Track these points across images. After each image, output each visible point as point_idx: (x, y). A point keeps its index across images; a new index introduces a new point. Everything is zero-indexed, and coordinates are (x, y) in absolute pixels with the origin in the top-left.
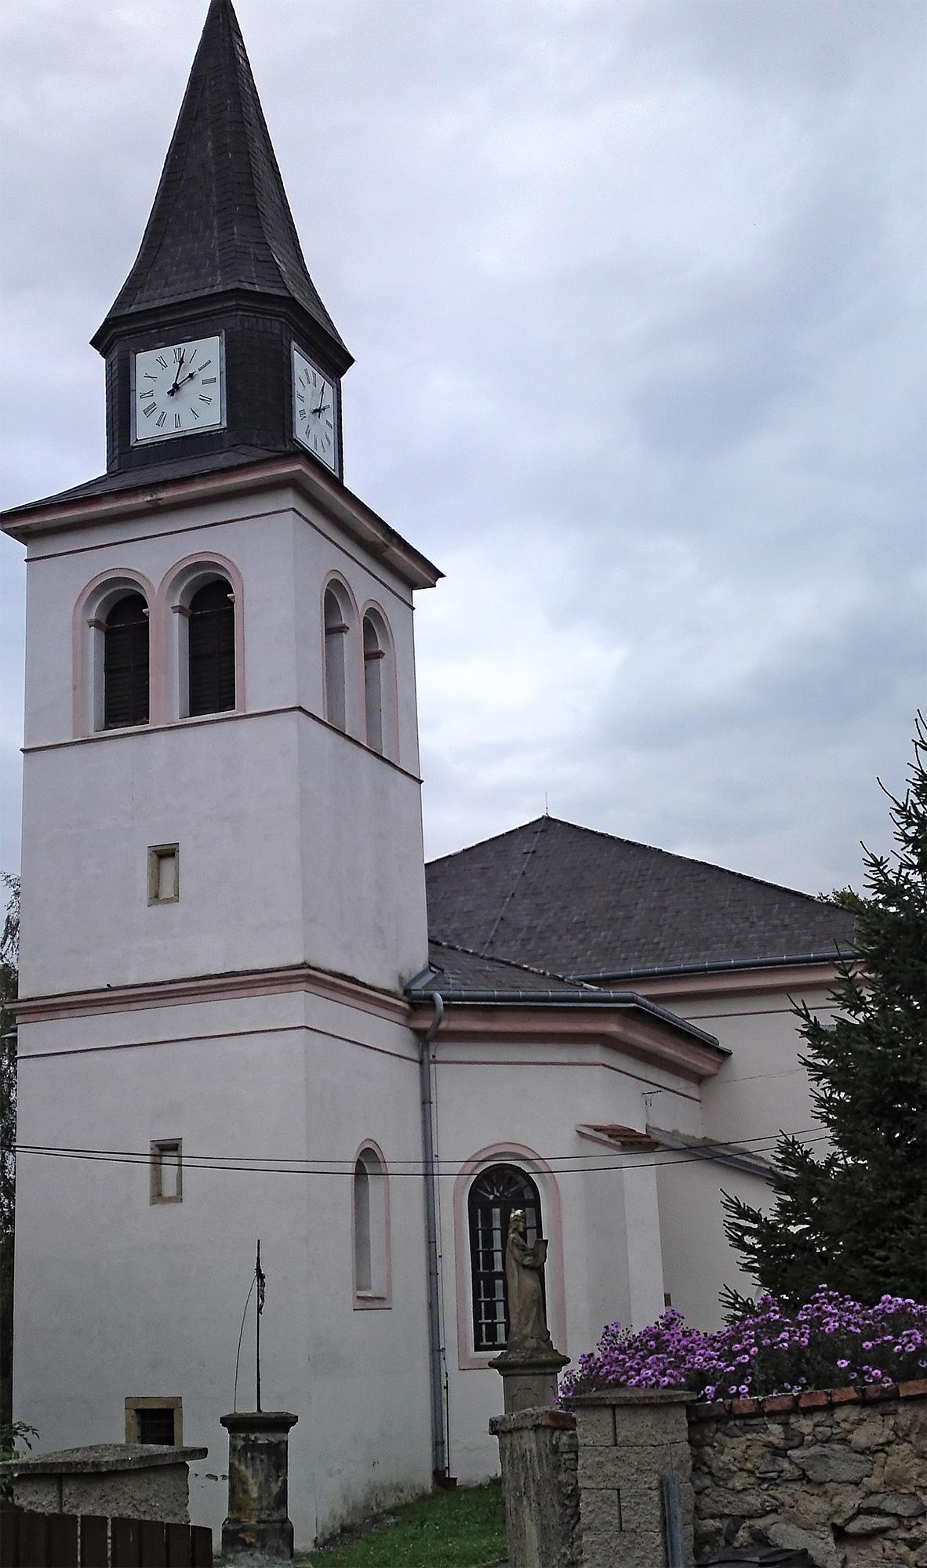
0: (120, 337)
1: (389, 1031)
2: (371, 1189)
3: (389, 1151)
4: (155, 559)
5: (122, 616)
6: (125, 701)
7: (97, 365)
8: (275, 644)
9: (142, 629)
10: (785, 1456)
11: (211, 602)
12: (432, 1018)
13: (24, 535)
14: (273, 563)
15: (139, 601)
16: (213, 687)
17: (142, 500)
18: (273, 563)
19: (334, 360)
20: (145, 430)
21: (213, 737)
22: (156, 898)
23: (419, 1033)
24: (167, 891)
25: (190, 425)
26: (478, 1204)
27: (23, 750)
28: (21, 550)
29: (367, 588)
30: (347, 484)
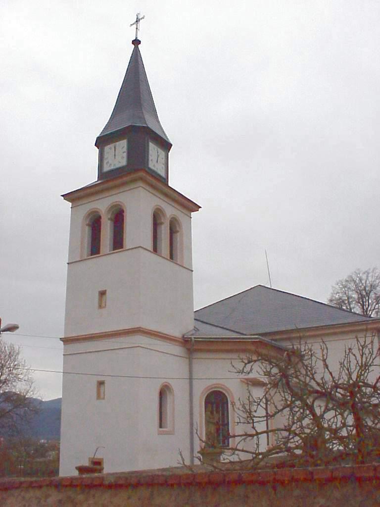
0: (101, 142)
1: (178, 350)
2: (168, 398)
3: (173, 383)
4: (103, 205)
5: (95, 224)
6: (95, 249)
7: (96, 151)
8: (138, 229)
9: (100, 226)
10: (322, 416)
11: (119, 218)
12: (192, 346)
13: (71, 201)
14: (139, 204)
15: (100, 217)
16: (118, 243)
17: (332, 331)
18: (139, 204)
19: (166, 146)
20: (106, 168)
21: (118, 257)
22: (100, 307)
23: (189, 350)
24: (103, 305)
25: (118, 165)
26: (207, 402)
27: (68, 263)
28: (70, 204)
29: (170, 211)
30: (169, 185)
